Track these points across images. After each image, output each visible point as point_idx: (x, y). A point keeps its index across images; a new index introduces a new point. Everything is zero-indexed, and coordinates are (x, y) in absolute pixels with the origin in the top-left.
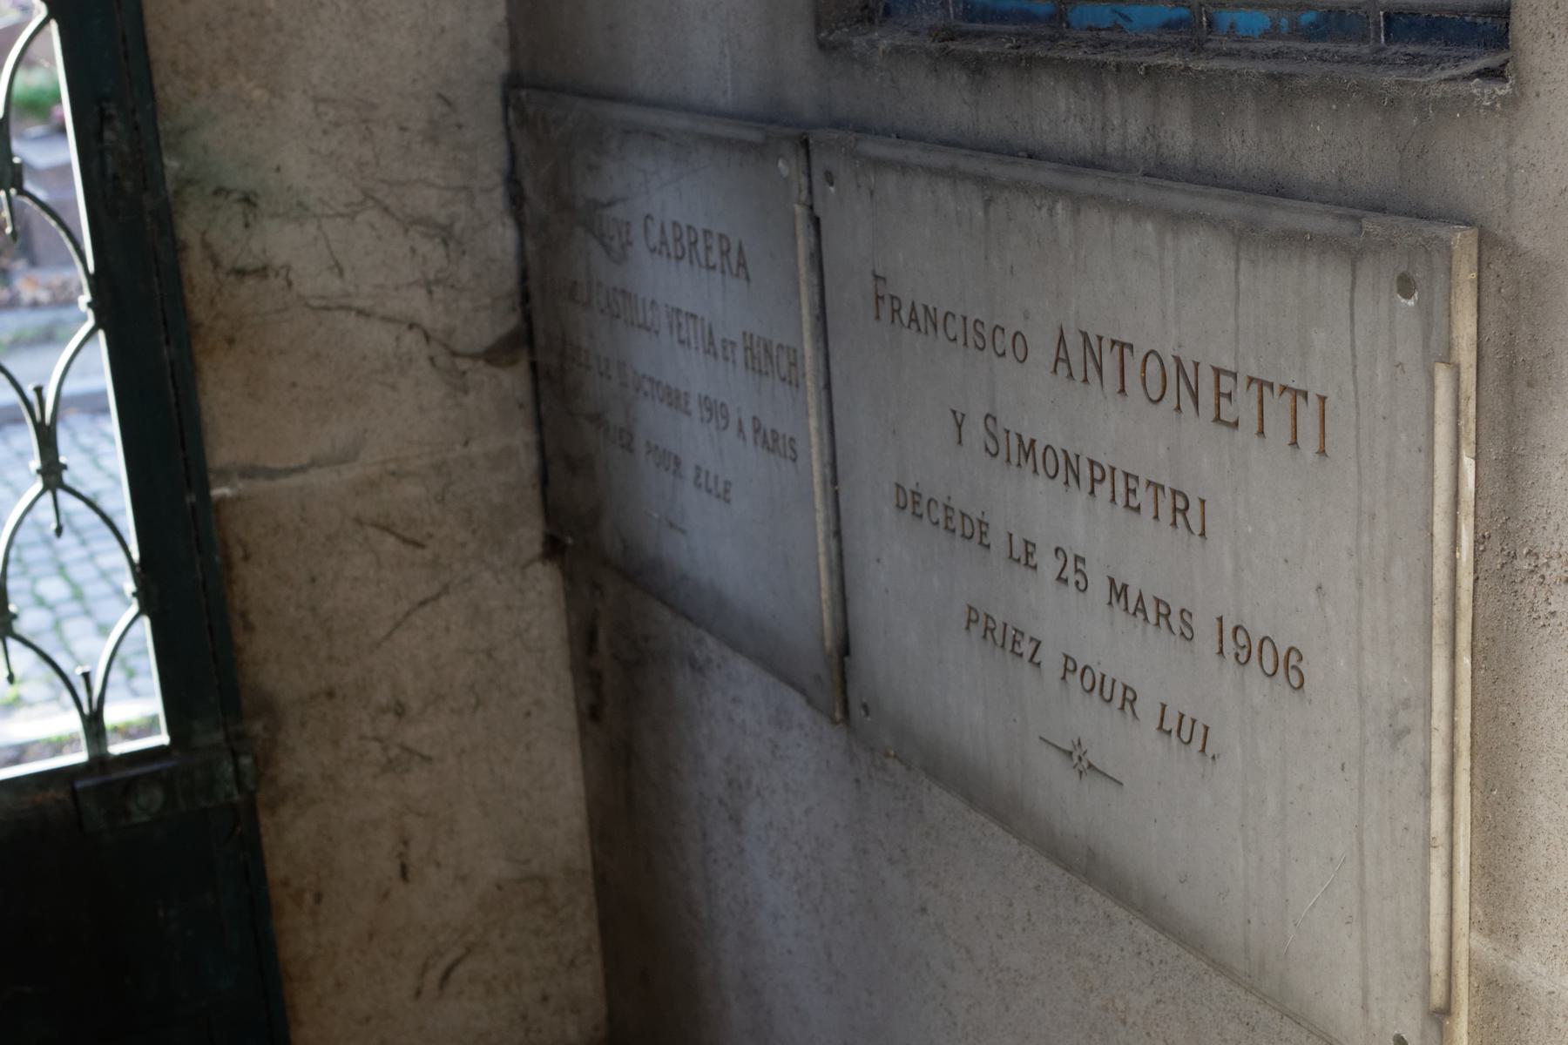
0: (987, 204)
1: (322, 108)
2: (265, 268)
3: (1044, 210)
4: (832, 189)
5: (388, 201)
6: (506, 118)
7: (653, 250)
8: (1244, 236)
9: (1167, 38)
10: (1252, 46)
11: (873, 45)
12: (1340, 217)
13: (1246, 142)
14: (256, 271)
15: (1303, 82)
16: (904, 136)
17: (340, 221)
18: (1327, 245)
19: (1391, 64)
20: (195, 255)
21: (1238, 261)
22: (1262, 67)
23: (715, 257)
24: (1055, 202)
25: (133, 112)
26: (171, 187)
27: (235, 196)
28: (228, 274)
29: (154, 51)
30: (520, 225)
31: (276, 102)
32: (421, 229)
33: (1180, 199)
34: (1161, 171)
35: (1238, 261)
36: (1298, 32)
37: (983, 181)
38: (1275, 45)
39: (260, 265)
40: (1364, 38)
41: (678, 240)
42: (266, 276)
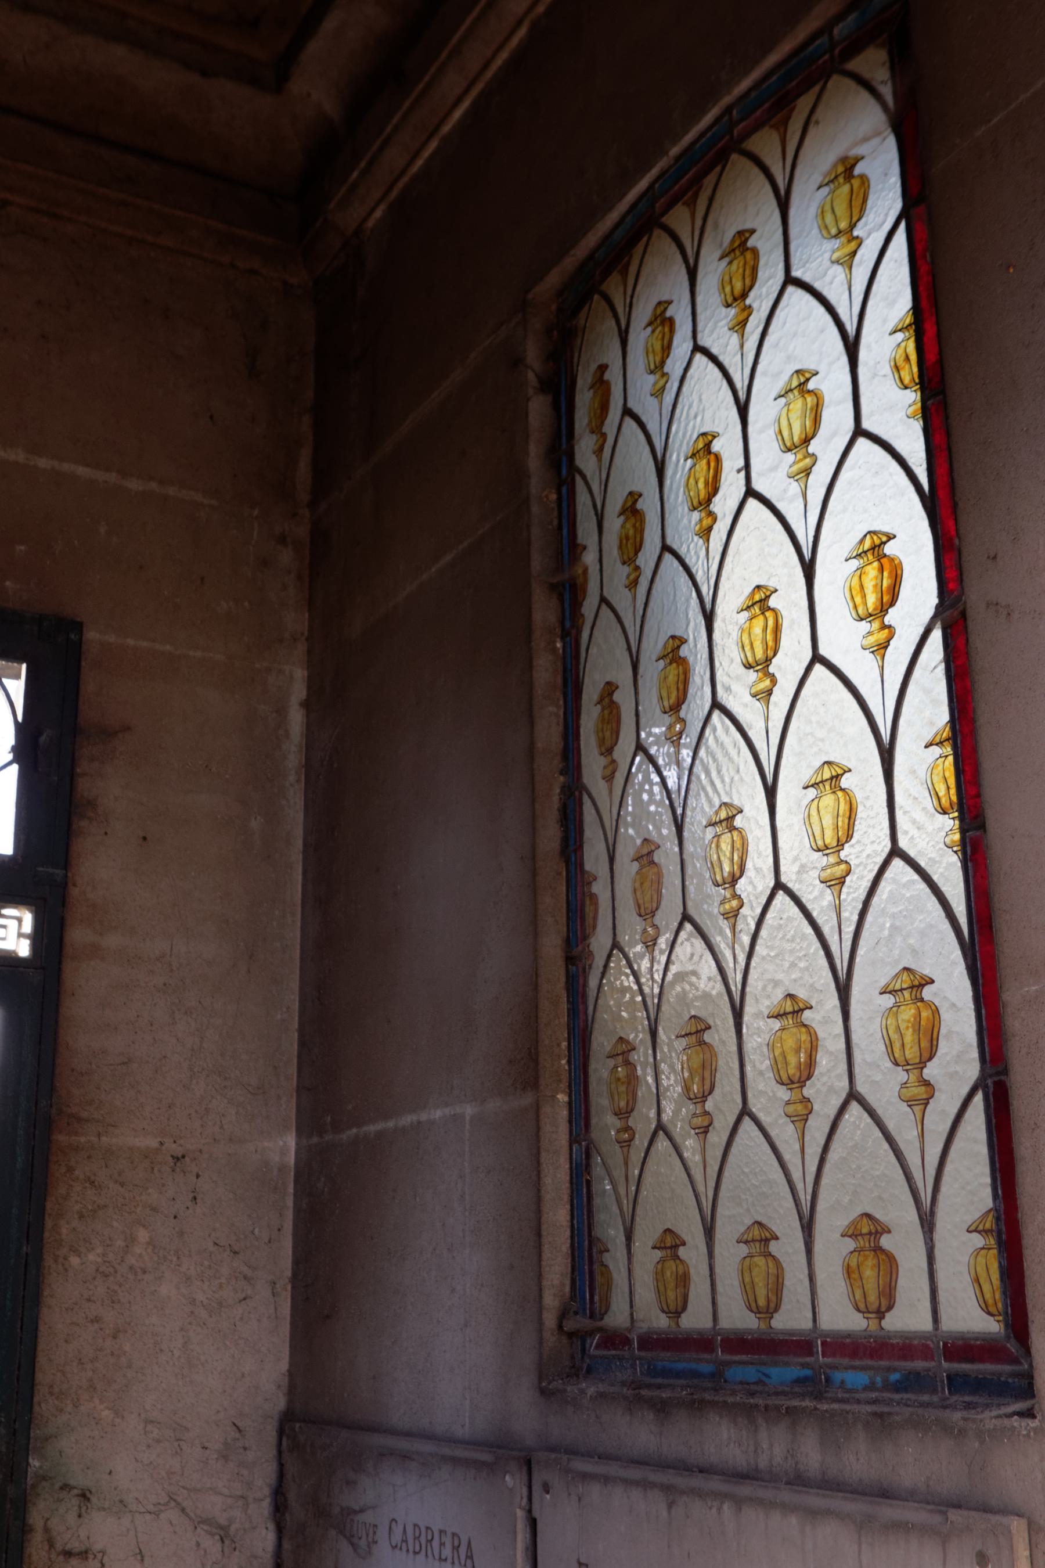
0: (670, 1505)
1: (149, 1427)
2: (86, 1552)
3: (714, 1510)
4: (548, 1496)
5: (185, 1504)
6: (280, 1444)
7: (394, 1547)
8: (864, 1525)
9: (797, 1389)
10: (857, 1396)
11: (583, 1392)
12: (931, 1511)
13: (860, 1459)
14: (80, 1554)
15: (898, 1418)
16: (605, 1457)
17: (148, 1516)
18: (924, 1530)
19: (953, 1407)
20: (37, 1538)
21: (860, 1544)
22: (869, 1408)
23: (447, 1552)
24: (722, 1503)
25: (15, 1421)
26: (30, 1481)
27: (76, 1491)
28: (58, 1555)
29: (39, 1376)
30: (280, 1530)
31: (118, 1420)
32: (205, 1527)
33: (815, 1500)
34: (799, 1480)
35: (860, 1544)
36: (888, 1386)
37: (667, 1489)
38: (874, 1395)
39: (83, 1548)
40: (935, 1391)
41: (416, 1538)
42: (87, 1558)
